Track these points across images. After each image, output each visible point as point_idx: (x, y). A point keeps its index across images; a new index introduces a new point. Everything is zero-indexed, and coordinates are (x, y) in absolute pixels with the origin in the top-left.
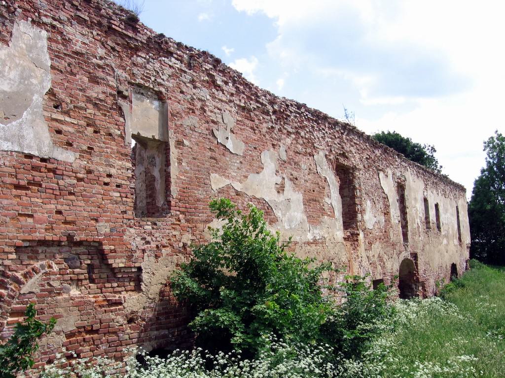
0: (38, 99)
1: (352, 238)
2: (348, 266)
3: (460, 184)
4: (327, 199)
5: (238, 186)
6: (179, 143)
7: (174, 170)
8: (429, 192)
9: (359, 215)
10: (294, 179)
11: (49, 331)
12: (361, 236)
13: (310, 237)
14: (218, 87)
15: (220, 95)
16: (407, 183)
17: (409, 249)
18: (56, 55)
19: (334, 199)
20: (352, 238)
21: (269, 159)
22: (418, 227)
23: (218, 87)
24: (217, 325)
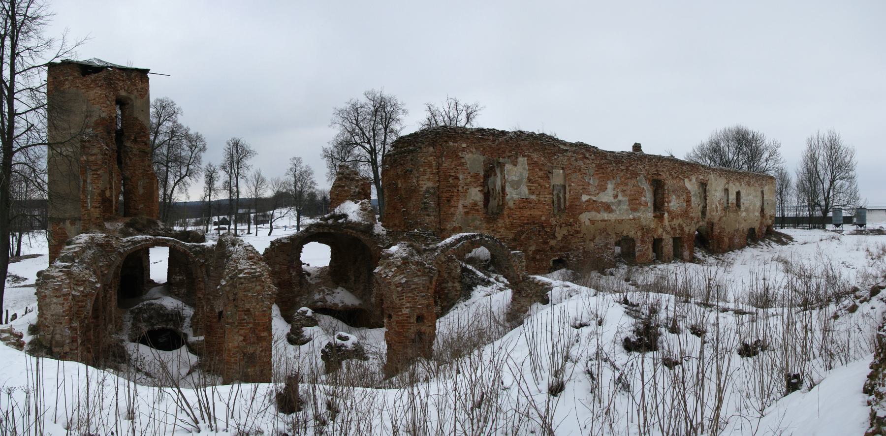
0: (525, 180)
1: (659, 217)
2: (655, 230)
3: (328, 170)
4: (643, 198)
5: (594, 198)
6: (570, 185)
7: (567, 196)
8: (731, 184)
9: (666, 204)
10: (623, 191)
11: (600, 234)
12: (666, 215)
13: (631, 217)
14: (587, 158)
15: (588, 161)
16: (709, 182)
17: (706, 220)
18: (529, 165)
19: (648, 197)
20: (659, 217)
21: (610, 186)
22: (717, 207)
23: (587, 158)
24: (202, 338)
